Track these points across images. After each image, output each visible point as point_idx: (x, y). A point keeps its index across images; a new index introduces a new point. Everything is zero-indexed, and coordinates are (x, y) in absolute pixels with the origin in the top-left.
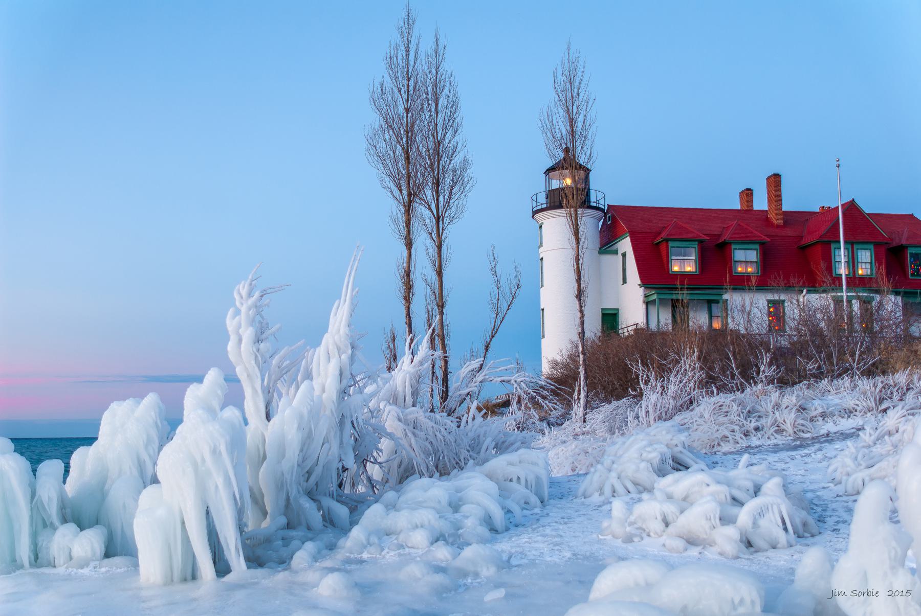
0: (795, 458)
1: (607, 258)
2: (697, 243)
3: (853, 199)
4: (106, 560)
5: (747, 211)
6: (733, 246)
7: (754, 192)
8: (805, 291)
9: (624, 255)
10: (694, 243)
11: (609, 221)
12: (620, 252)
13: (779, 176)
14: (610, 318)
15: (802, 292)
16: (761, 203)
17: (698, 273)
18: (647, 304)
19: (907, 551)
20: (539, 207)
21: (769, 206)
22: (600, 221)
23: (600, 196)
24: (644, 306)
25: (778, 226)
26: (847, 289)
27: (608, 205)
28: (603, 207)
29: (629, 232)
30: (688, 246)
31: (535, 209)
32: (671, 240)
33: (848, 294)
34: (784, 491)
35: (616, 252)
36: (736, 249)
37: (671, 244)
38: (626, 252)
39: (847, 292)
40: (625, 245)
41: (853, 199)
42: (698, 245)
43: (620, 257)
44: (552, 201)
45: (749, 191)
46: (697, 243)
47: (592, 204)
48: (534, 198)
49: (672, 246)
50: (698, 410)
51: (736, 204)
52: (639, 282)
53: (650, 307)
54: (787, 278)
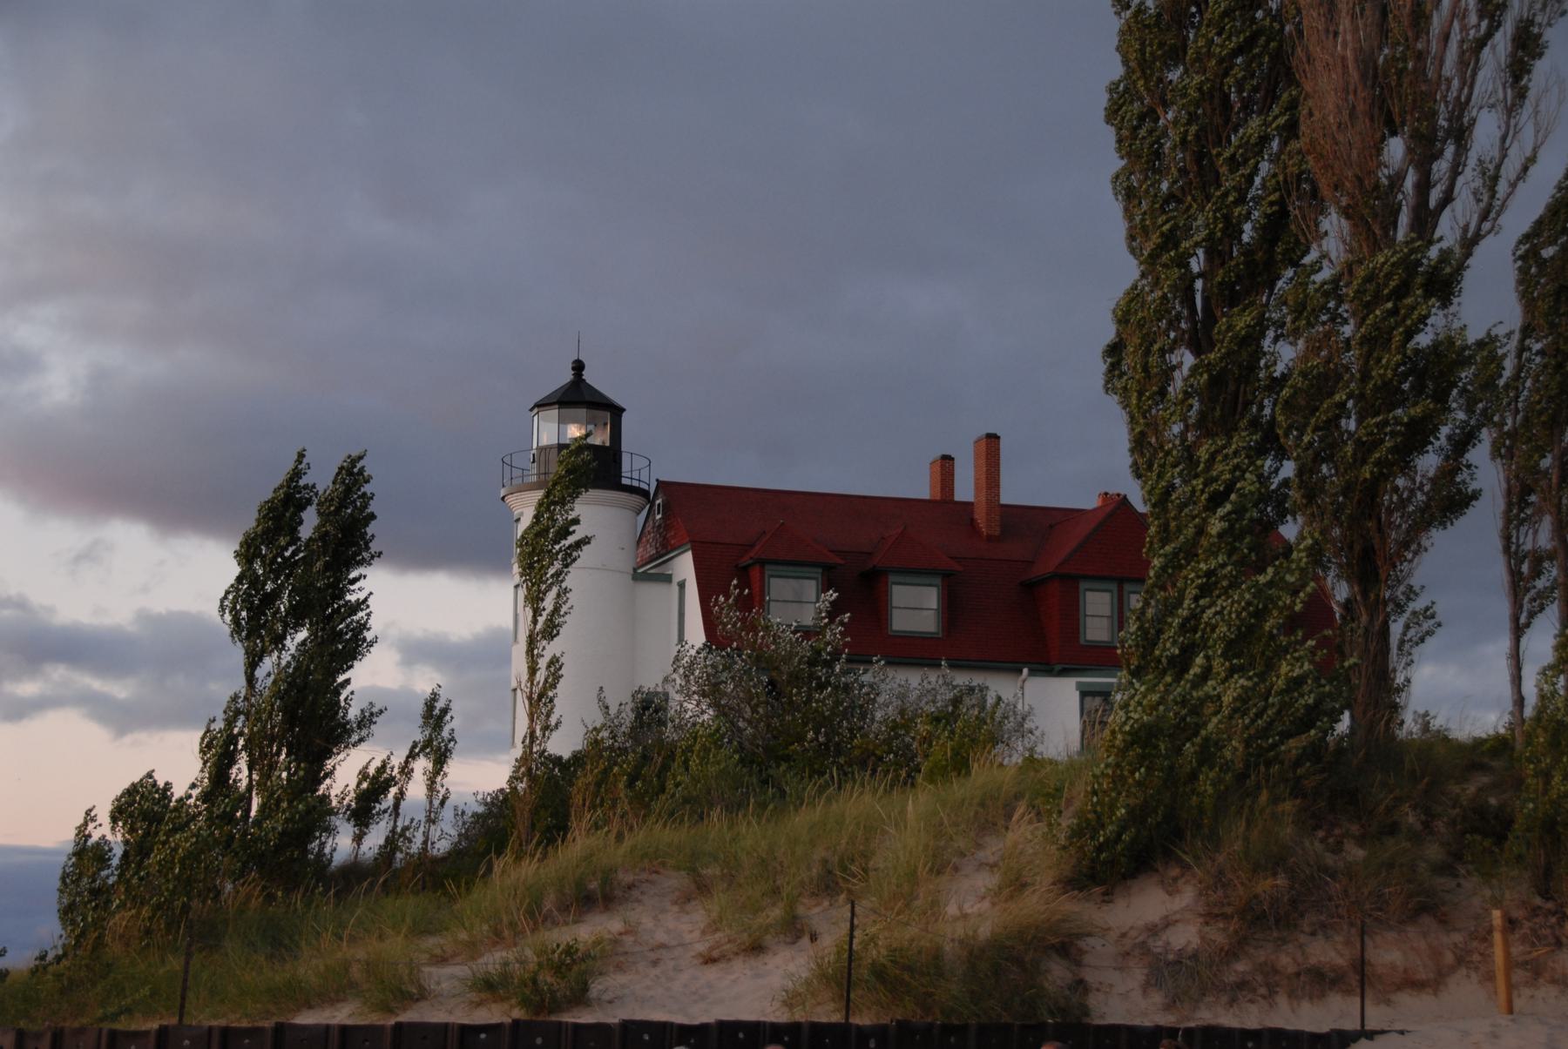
1: (651, 593)
2: (820, 570)
3: (1481, 490)
5: (944, 506)
6: (892, 578)
7: (956, 461)
8: (1025, 671)
9: (682, 585)
10: (815, 570)
11: (659, 513)
12: (676, 580)
13: (998, 438)
15: (1021, 672)
16: (965, 489)
17: (940, 636)
20: (635, 484)
21: (976, 496)
22: (638, 514)
23: (640, 463)
25: (990, 538)
27: (657, 480)
28: (646, 487)
30: (784, 574)
32: (1086, 578)
35: (668, 579)
36: (772, 576)
37: (769, 570)
38: (685, 580)
40: (684, 566)
41: (1481, 490)
42: (823, 575)
43: (675, 588)
44: (542, 471)
45: (947, 460)
46: (820, 570)
47: (625, 481)
48: (507, 460)
49: (770, 573)
50: (221, 712)
51: (919, 487)
54: (1399, 690)
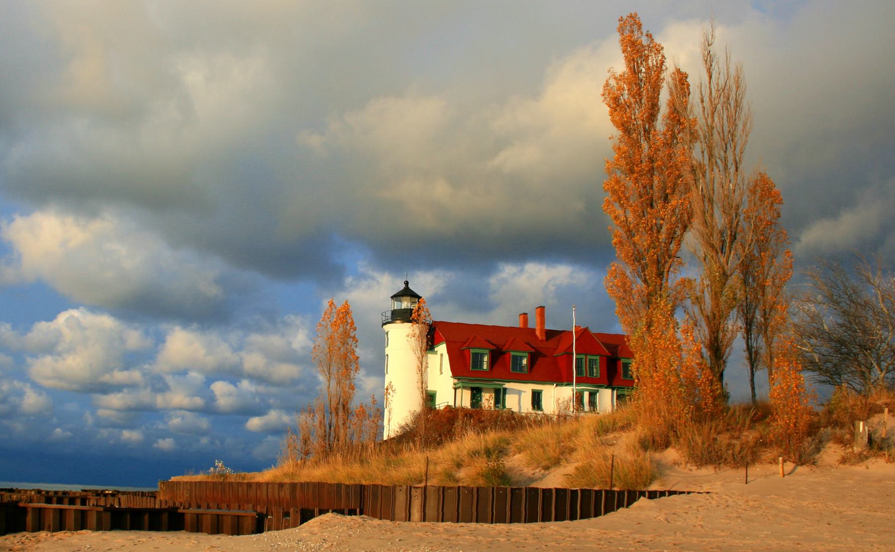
0: (781, 209)
1: (430, 356)
4: (841, 466)
9: (442, 355)
12: (439, 353)
14: (430, 398)
18: (455, 389)
19: (219, 380)
24: (454, 390)
26: (576, 384)
29: (446, 341)
31: (384, 322)
33: (577, 388)
34: (734, 469)
39: (576, 386)
40: (442, 348)
41: (587, 327)
43: (438, 356)
51: (517, 323)
52: (451, 375)
53: (457, 390)
